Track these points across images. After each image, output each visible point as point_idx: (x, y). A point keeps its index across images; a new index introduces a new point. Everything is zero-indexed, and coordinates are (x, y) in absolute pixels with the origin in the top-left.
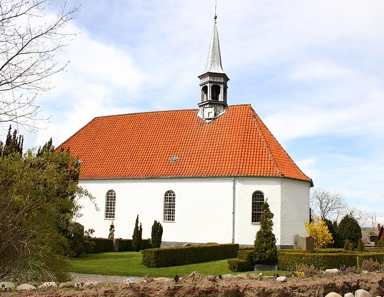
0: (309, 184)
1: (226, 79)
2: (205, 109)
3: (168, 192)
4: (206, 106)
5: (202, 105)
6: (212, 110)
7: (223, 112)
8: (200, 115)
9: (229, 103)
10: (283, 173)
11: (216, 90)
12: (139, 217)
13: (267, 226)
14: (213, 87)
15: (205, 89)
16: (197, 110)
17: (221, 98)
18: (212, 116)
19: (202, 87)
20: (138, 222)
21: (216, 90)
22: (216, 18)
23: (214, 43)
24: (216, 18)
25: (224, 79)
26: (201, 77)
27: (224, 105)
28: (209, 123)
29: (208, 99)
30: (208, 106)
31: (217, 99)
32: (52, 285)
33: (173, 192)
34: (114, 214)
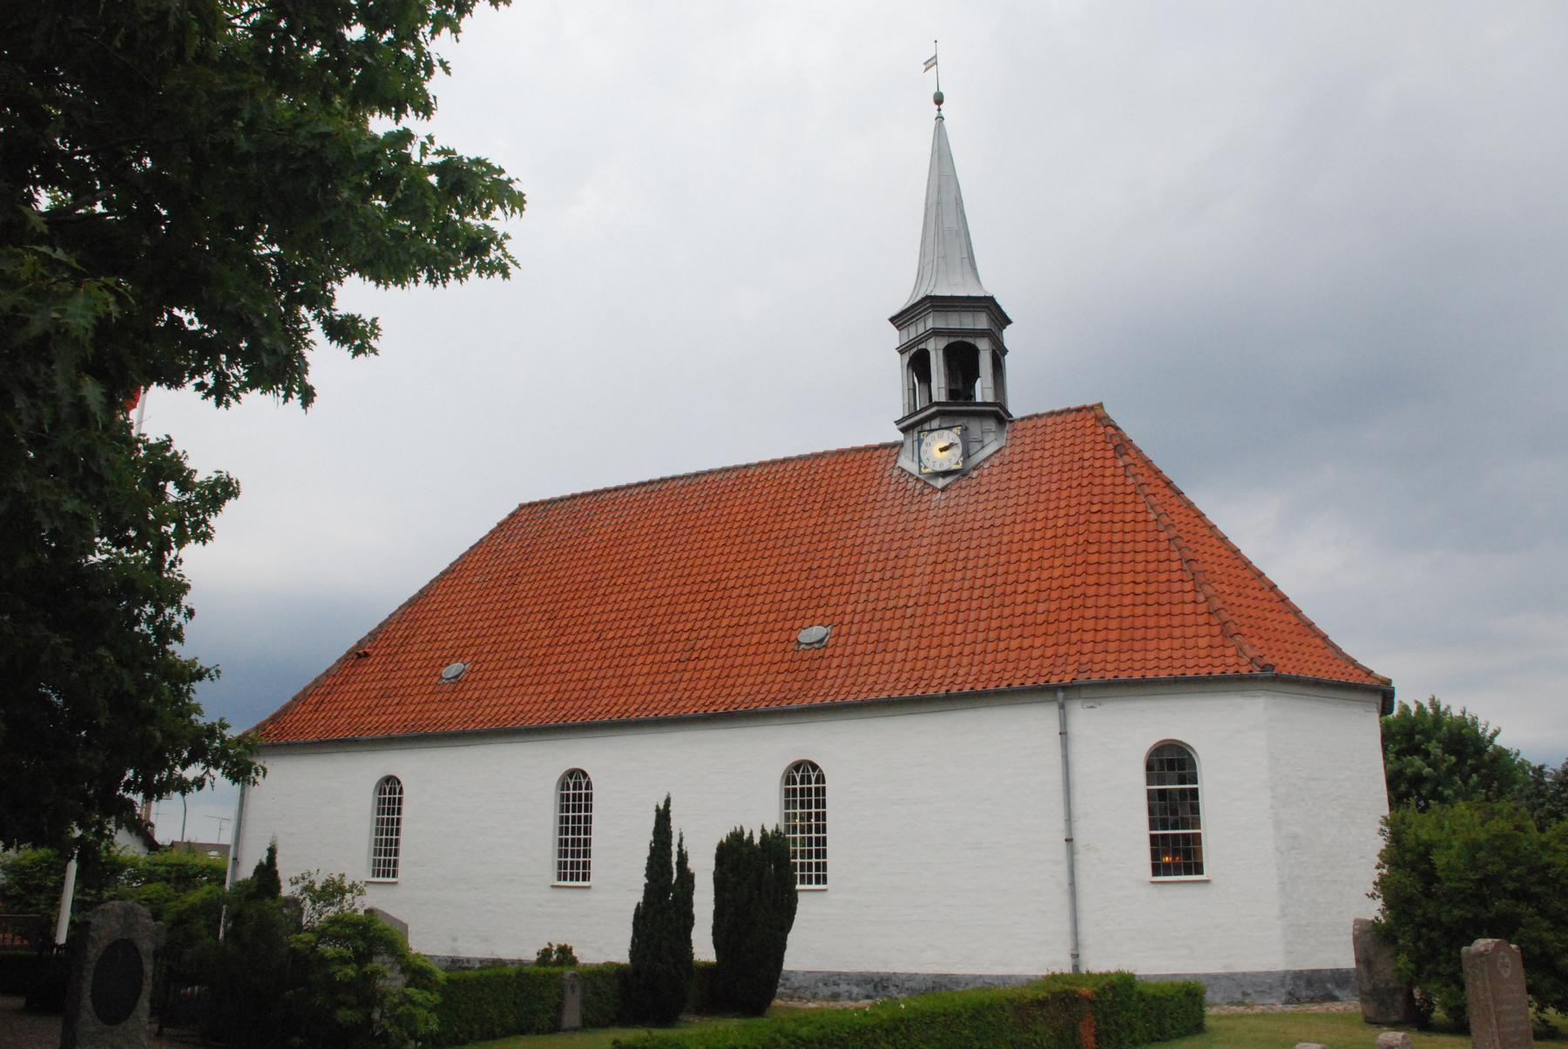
0: (1379, 700)
1: (1002, 320)
2: (928, 439)
3: (797, 766)
4: (927, 427)
5: (914, 425)
6: (951, 436)
7: (992, 443)
8: (906, 462)
9: (1017, 408)
10: (1267, 660)
11: (962, 362)
12: (684, 835)
13: (919, 437)
14: (949, 352)
15: (919, 364)
16: (894, 445)
17: (983, 390)
18: (951, 460)
19: (906, 358)
20: (669, 835)
21: (962, 362)
22: (939, 100)
23: (939, 193)
24: (939, 100)
25: (991, 320)
26: (900, 320)
27: (998, 414)
28: (943, 490)
29: (935, 398)
30: (935, 424)
31: (969, 395)
32: (231, 270)
33: (815, 767)
34: (586, 865)
